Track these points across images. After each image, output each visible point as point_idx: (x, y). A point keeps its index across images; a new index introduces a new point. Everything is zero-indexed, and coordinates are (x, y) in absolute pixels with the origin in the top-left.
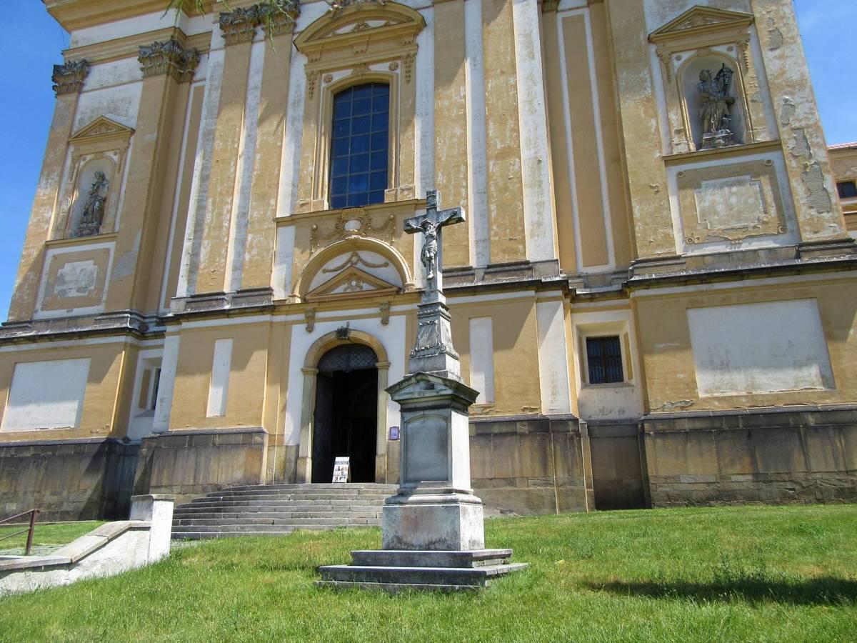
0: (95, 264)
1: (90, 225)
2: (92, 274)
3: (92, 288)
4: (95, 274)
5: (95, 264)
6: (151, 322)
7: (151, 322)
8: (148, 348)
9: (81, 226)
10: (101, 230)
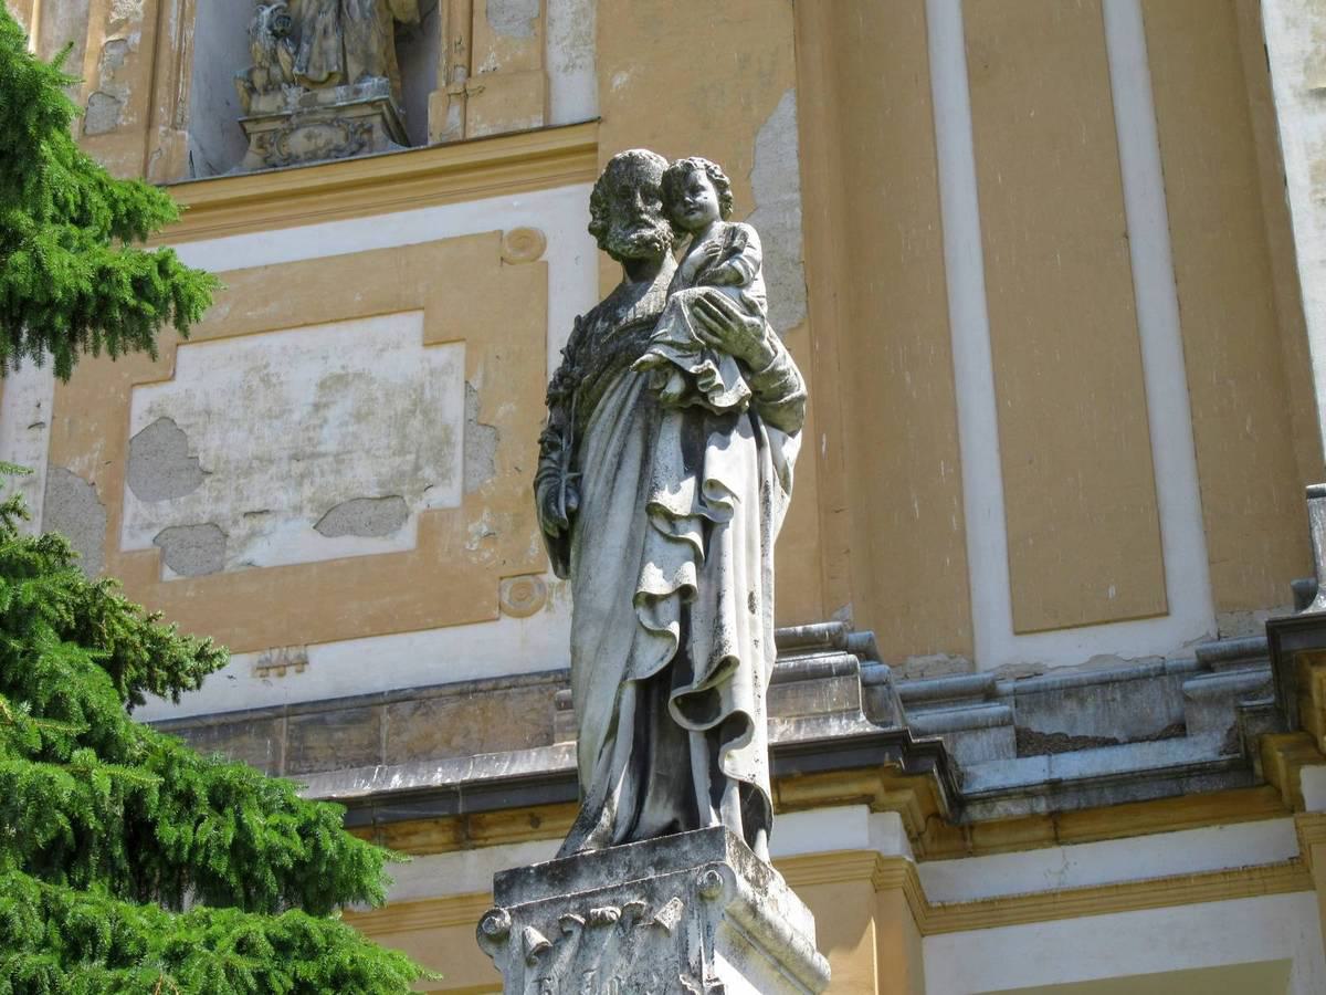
0: (432, 341)
1: (335, 95)
2: (423, 407)
3: (446, 495)
4: (453, 408)
5: (432, 341)
6: (975, 727)
7: (975, 727)
8: (994, 912)
9: (263, 104)
10: (441, 116)
